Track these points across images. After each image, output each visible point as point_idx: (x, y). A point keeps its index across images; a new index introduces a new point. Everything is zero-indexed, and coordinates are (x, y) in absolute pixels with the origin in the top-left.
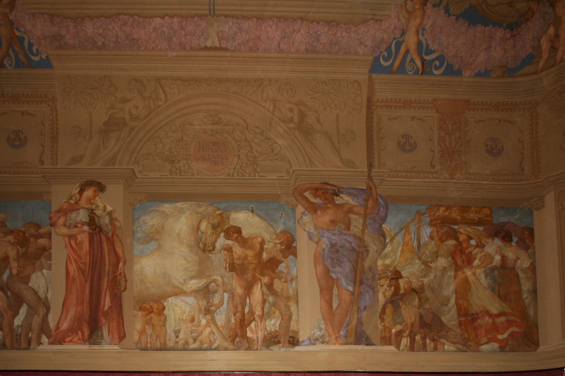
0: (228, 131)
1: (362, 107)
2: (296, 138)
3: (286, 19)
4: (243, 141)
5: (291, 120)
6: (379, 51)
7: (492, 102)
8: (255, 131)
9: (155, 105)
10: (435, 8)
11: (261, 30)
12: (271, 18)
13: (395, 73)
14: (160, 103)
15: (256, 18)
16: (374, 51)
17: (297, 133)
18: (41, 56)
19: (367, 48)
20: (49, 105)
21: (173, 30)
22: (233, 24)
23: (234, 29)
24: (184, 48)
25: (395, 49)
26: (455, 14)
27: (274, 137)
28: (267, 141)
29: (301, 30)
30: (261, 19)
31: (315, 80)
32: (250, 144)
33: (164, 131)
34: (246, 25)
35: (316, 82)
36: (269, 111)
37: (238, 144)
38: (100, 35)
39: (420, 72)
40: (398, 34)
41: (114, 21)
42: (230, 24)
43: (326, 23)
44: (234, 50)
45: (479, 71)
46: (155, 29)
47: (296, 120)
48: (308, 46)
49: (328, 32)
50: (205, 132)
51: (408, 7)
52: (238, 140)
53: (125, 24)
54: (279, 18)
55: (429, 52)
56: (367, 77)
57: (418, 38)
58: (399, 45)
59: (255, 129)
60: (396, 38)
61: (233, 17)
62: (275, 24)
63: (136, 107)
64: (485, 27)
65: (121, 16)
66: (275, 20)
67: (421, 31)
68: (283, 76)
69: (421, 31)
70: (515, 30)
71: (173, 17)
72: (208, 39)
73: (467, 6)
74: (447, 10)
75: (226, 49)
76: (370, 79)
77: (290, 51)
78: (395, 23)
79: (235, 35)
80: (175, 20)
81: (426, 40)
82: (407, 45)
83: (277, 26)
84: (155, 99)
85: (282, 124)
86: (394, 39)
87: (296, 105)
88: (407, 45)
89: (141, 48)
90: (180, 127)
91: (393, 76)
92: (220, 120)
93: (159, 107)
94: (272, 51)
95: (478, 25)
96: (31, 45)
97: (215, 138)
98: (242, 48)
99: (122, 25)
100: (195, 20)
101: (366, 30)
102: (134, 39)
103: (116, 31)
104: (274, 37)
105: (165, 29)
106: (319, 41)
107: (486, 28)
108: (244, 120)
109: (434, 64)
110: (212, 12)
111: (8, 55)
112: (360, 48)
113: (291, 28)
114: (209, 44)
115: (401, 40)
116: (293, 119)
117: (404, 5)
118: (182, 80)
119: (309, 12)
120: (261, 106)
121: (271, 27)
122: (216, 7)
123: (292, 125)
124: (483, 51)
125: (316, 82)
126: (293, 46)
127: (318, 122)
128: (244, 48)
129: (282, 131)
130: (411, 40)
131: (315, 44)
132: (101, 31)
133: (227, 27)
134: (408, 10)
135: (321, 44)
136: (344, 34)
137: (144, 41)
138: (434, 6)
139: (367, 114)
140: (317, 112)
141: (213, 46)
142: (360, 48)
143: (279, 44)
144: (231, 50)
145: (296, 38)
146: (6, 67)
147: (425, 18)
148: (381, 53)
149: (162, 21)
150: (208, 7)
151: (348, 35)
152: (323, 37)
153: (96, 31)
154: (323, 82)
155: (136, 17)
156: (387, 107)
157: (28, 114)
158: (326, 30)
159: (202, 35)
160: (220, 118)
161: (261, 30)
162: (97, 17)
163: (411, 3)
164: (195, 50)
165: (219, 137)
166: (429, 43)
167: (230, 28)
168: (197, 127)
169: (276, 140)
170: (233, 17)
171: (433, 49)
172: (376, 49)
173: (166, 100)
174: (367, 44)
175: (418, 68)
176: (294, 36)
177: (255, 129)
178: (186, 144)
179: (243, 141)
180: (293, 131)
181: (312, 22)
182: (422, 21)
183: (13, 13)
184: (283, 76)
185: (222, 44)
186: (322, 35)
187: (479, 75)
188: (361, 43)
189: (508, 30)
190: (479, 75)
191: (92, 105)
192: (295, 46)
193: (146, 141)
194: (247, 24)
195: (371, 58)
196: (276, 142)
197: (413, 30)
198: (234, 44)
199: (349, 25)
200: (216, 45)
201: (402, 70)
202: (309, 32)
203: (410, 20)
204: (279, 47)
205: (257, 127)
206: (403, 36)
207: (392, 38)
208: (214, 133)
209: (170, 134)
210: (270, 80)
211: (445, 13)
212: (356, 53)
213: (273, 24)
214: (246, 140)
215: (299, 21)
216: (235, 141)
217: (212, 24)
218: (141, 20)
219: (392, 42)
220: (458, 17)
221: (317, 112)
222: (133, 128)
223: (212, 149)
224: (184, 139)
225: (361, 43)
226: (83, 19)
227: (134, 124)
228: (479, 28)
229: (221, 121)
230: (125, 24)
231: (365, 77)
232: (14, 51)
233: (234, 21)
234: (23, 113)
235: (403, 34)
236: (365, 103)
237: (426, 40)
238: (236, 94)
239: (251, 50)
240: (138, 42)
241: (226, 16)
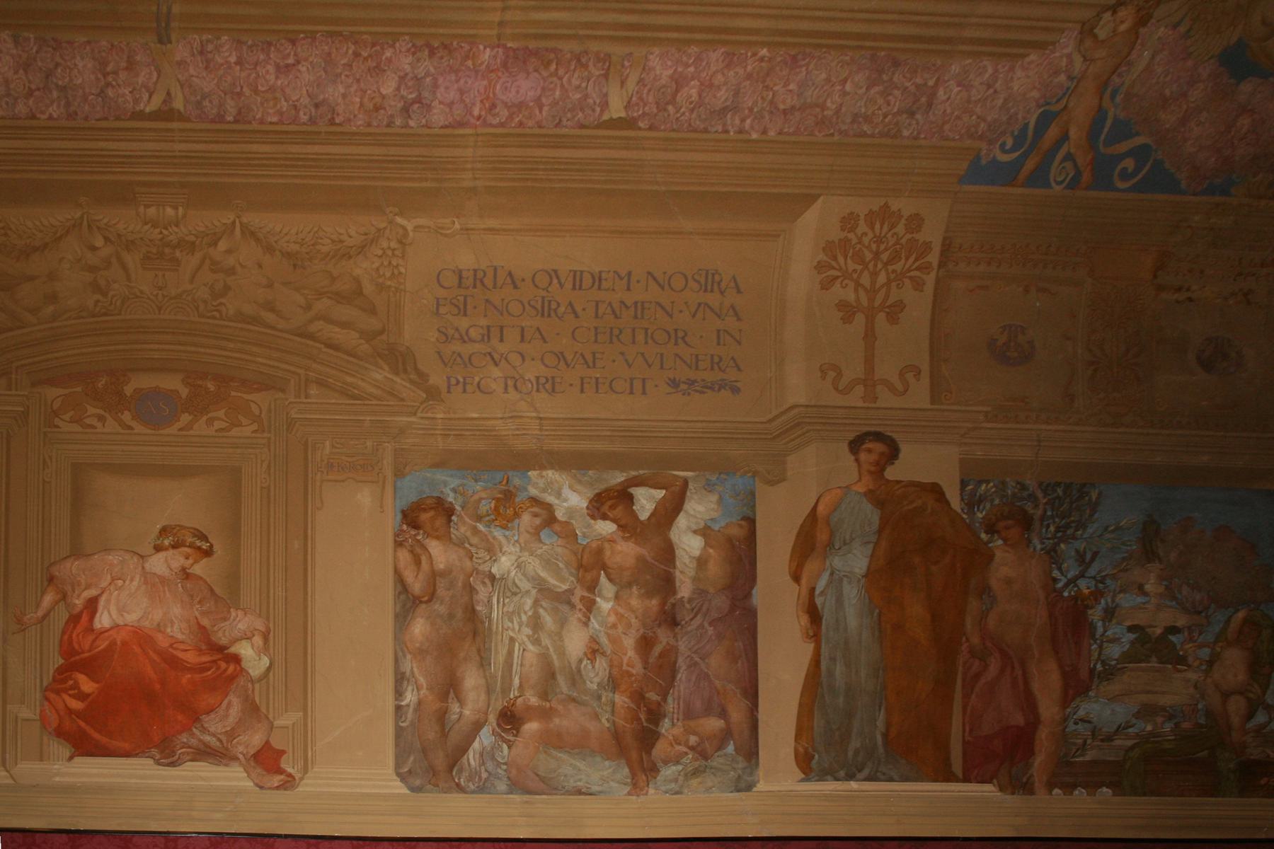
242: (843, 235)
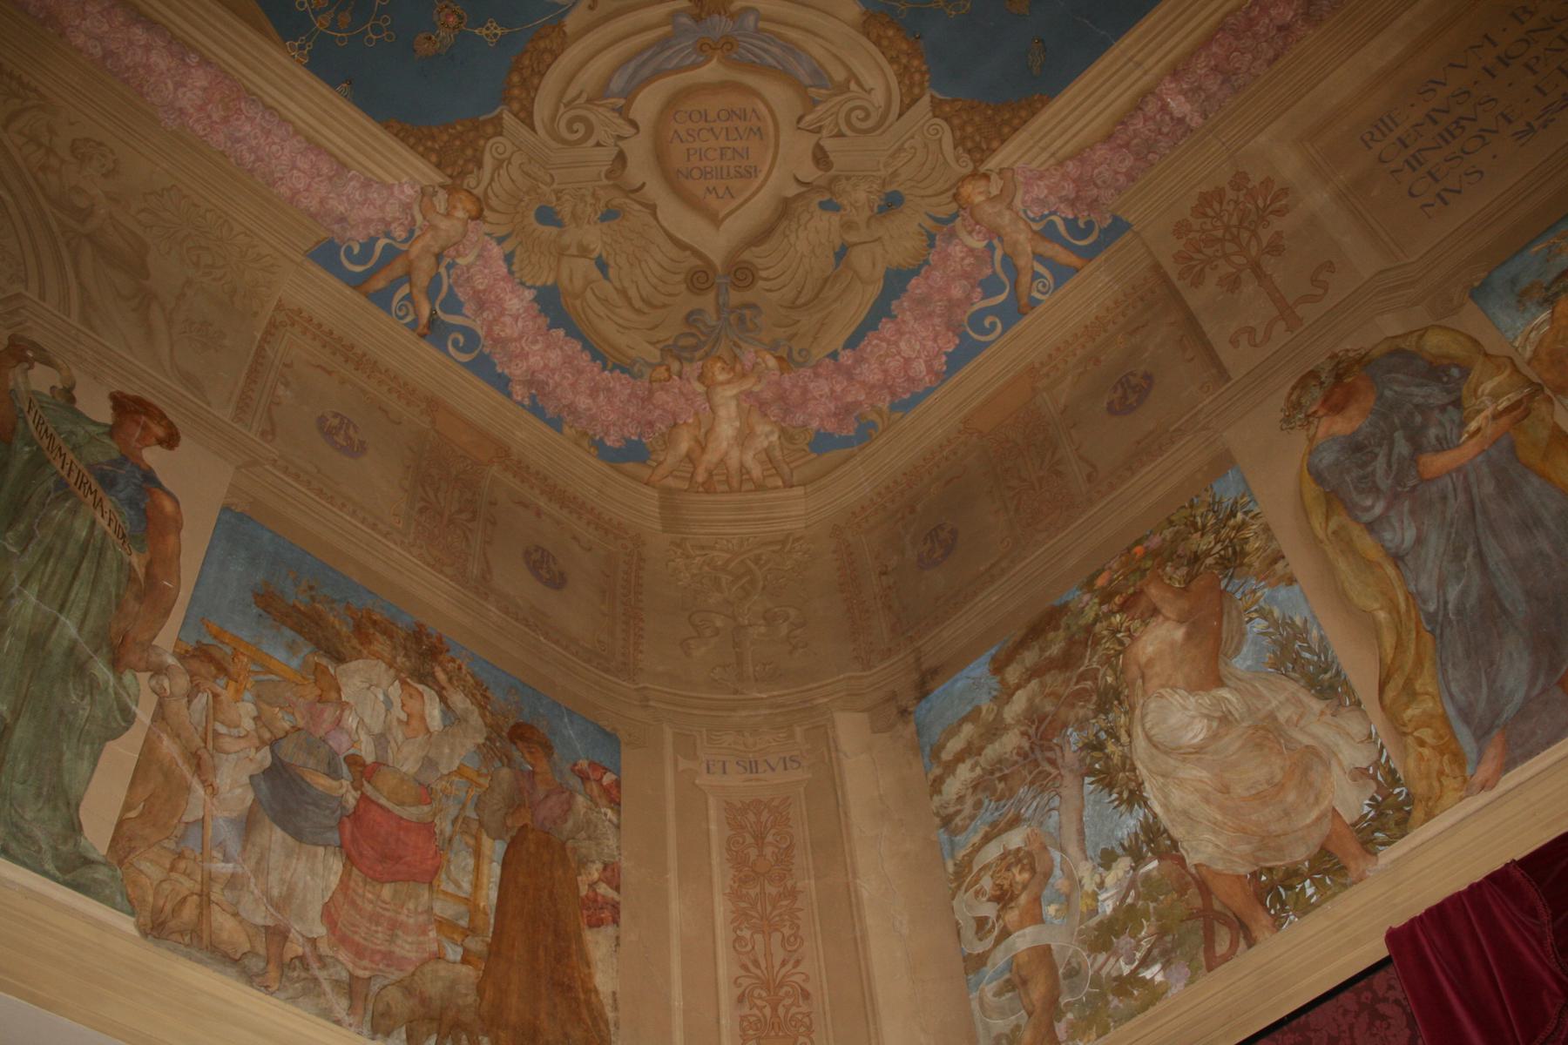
146: (1039, 302)
242: (1184, 241)
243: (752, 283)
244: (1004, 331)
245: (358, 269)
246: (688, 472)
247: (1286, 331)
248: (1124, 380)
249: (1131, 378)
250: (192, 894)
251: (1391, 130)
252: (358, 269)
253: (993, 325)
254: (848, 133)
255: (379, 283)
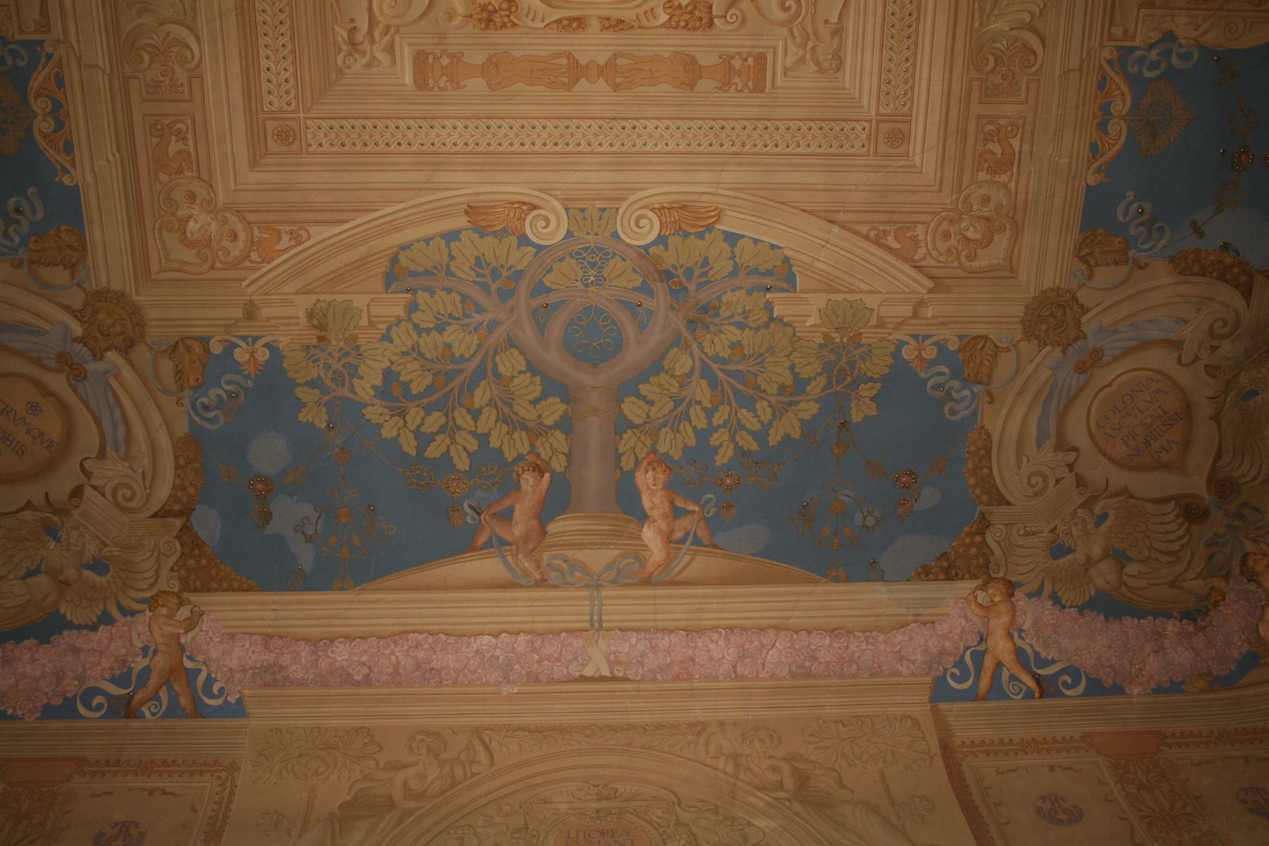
0: (634, 810)
1: (931, 757)
2: (798, 815)
3: (744, 629)
4: (672, 825)
5: (780, 786)
6: (941, 668)
7: (1212, 732)
8: (699, 808)
9: (465, 775)
10: (1033, 600)
11: (696, 647)
12: (714, 629)
13: (984, 699)
14: (476, 768)
15: (684, 630)
16: (930, 668)
17: (797, 806)
18: (226, 698)
19: (916, 665)
20: (219, 778)
21: (516, 654)
22: (638, 640)
23: (642, 648)
24: (537, 680)
25: (974, 666)
26: (1074, 604)
27: (743, 816)
28: (729, 823)
29: (777, 644)
30: (692, 631)
31: (819, 719)
32: (690, 830)
33: (484, 816)
34: (665, 641)
35: (821, 721)
36: (725, 773)
37: (661, 830)
38: (363, 664)
39: (1037, 695)
40: (972, 640)
41: (395, 643)
42: (633, 641)
43: (826, 632)
44: (642, 680)
45: (1159, 685)
46: (477, 652)
47: (789, 783)
48: (794, 668)
49: (831, 645)
50: (580, 814)
51: (980, 600)
52: (658, 824)
53: (417, 647)
54: (731, 629)
55: (1046, 663)
56: (929, 708)
57: (1014, 644)
58: (978, 657)
59: (699, 804)
60: (970, 647)
61: (638, 630)
62: (722, 638)
63: (422, 777)
64: (1139, 620)
65: (411, 635)
66: (723, 632)
67: (1016, 634)
68: (748, 715)
69: (1016, 634)
70: (1199, 620)
71: (518, 633)
72: (586, 664)
73: (1093, 593)
74: (1056, 600)
75: (625, 679)
76: (935, 712)
77: (757, 676)
78: (960, 624)
79: (642, 656)
80: (521, 638)
81: (1031, 646)
82: (995, 657)
83: (729, 640)
84: (467, 764)
85: (758, 793)
86: (966, 648)
87: (785, 760)
88: (995, 657)
89: (445, 682)
90: (521, 807)
91: (981, 704)
92: (615, 793)
93: (473, 775)
94: (721, 678)
95: (1123, 618)
96: (210, 681)
97: (604, 823)
98: (658, 676)
99: (410, 648)
100: (562, 638)
101: (907, 638)
102: (433, 669)
103: (397, 658)
104: (723, 658)
105: (498, 652)
106: (815, 659)
107: (1142, 621)
108: (674, 793)
109: (1060, 683)
110: (596, 625)
111: (155, 696)
112: (902, 665)
113: (757, 643)
114: (588, 672)
115: (981, 648)
116: (782, 784)
117: (971, 598)
118: (530, 731)
119: (789, 618)
120: (706, 765)
121: (717, 642)
122: (604, 618)
123: (782, 794)
124: (1152, 655)
125: (821, 721)
126: (764, 669)
127: (841, 784)
128: (662, 677)
129: (761, 804)
130: (1001, 647)
131: (807, 664)
132: (364, 659)
133: (627, 645)
134: (981, 605)
135: (821, 663)
136: (864, 646)
137: (452, 672)
138: (1030, 596)
139: (947, 766)
140: (835, 770)
141: (597, 675)
142: (902, 665)
143: (735, 667)
144: (635, 680)
145: (769, 657)
146: (143, 716)
147: (1018, 613)
148: (946, 670)
149: (494, 640)
150: (588, 618)
151: (873, 648)
152: (823, 652)
153: (355, 658)
154: (836, 722)
155: (442, 636)
156: (987, 753)
157: (164, 792)
158: (827, 642)
159: (576, 659)
160: (617, 790)
161: (696, 647)
162: (361, 638)
163: (984, 594)
164: (559, 682)
165: (615, 820)
166: (1038, 649)
167: (632, 647)
168: (563, 807)
169: (750, 819)
170: (638, 630)
171: (1050, 658)
172: (935, 665)
173: (492, 763)
174: (913, 658)
175: (1028, 687)
176: (763, 655)
177: (699, 804)
178: (535, 836)
179: (672, 825)
180: (787, 803)
181: (796, 632)
182: (1014, 616)
183: (190, 635)
184: (748, 715)
185: (616, 672)
186: (821, 651)
187: (1159, 690)
188: (901, 659)
189: (1185, 621)
190: (1159, 690)
191: (318, 775)
192: (766, 669)
193: (440, 833)
194: (667, 639)
195: (928, 679)
196: (750, 824)
197: (1000, 632)
198: (641, 671)
199: (872, 632)
200: (603, 674)
201: (996, 691)
202: (792, 647)
203: (989, 619)
204: (735, 672)
205: (701, 801)
206: (984, 643)
207: (962, 648)
208: (602, 815)
209: (497, 819)
210: (722, 724)
211: (1053, 605)
212: (897, 673)
213: (719, 638)
214: (678, 823)
215: (771, 632)
216: (653, 826)
217: (597, 642)
218: (451, 639)
219: (964, 653)
220: (1081, 610)
221: (835, 770)
222: (410, 812)
223: (599, 841)
224: (531, 827)
225: (901, 659)
226: (332, 641)
227: (412, 804)
228: (1128, 622)
229: (617, 795)
230: (417, 645)
231: (923, 708)
232: (170, 689)
233: (640, 637)
234: (151, 792)
235: (982, 640)
236: (936, 749)
237: (1031, 646)
238: (649, 748)
239: (677, 678)
240: (440, 673)
241: (623, 630)
243: (840, 628)
244: (102, 717)
245: (969, 683)
246: (586, 621)
247: (1211, 418)
248: (127, 824)
249: (133, 826)
250: (67, 602)
251: (1161, 436)
252: (969, 683)
253: (100, 707)
254: (109, 495)
255: (984, 684)
